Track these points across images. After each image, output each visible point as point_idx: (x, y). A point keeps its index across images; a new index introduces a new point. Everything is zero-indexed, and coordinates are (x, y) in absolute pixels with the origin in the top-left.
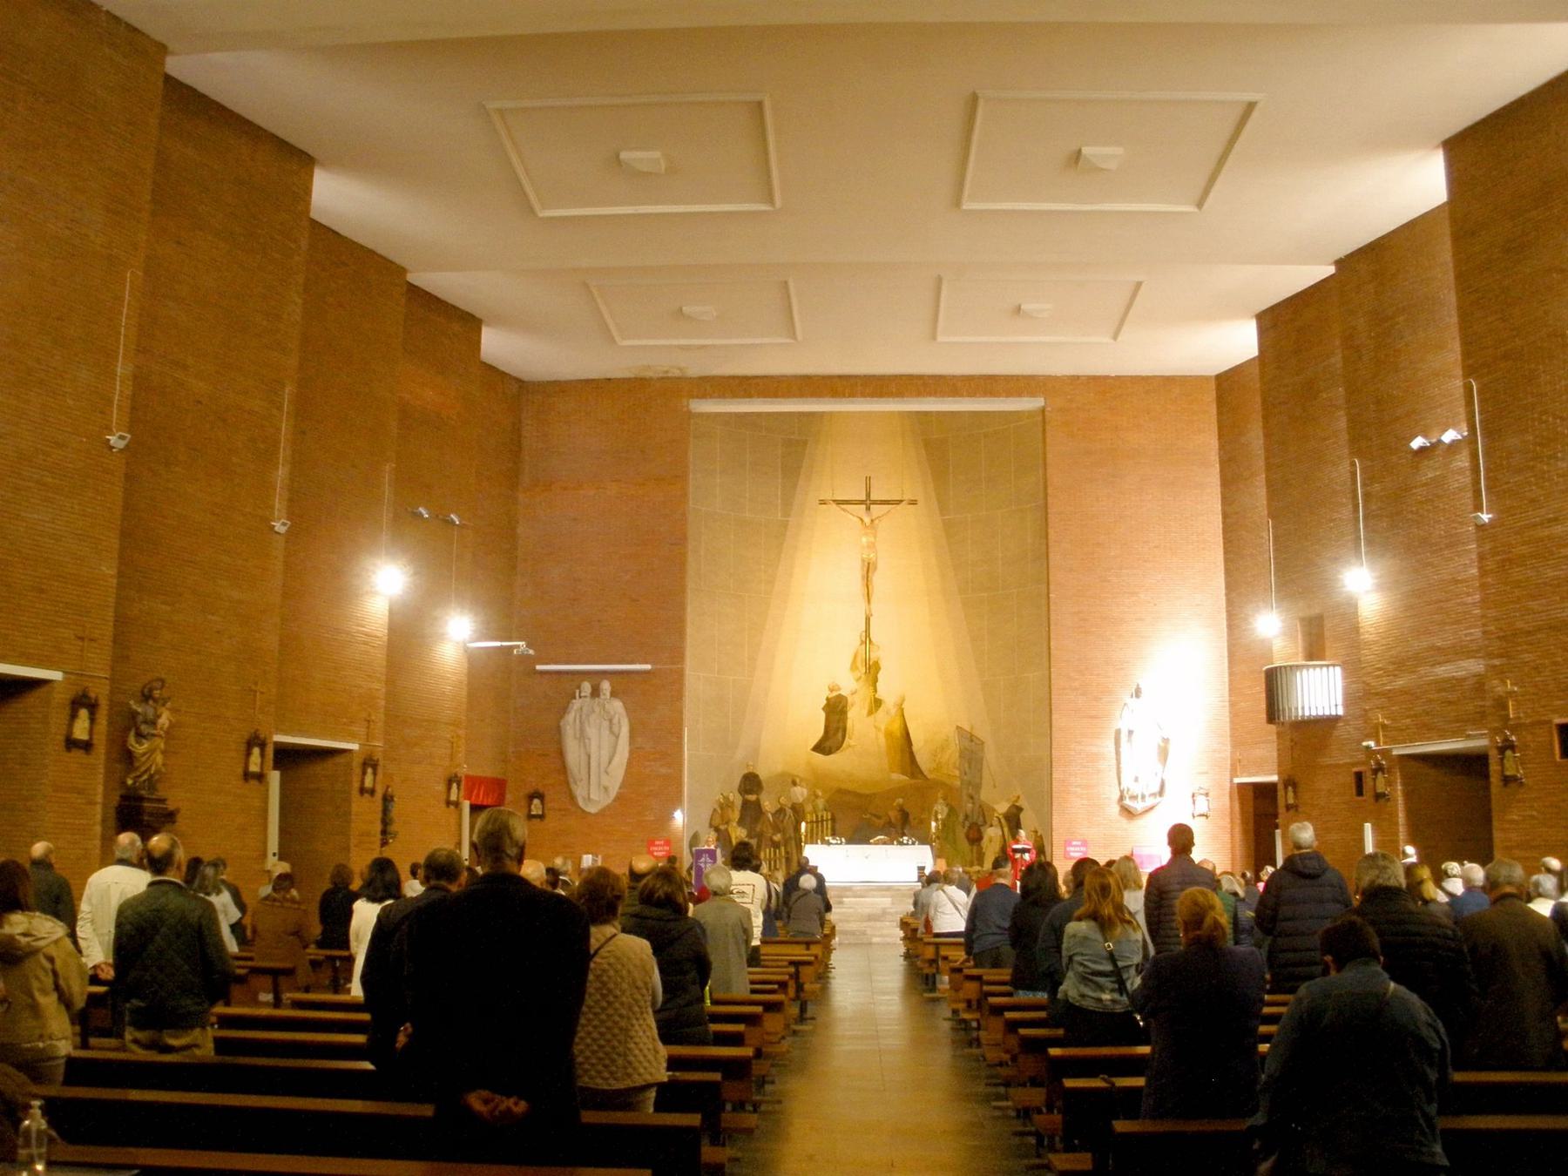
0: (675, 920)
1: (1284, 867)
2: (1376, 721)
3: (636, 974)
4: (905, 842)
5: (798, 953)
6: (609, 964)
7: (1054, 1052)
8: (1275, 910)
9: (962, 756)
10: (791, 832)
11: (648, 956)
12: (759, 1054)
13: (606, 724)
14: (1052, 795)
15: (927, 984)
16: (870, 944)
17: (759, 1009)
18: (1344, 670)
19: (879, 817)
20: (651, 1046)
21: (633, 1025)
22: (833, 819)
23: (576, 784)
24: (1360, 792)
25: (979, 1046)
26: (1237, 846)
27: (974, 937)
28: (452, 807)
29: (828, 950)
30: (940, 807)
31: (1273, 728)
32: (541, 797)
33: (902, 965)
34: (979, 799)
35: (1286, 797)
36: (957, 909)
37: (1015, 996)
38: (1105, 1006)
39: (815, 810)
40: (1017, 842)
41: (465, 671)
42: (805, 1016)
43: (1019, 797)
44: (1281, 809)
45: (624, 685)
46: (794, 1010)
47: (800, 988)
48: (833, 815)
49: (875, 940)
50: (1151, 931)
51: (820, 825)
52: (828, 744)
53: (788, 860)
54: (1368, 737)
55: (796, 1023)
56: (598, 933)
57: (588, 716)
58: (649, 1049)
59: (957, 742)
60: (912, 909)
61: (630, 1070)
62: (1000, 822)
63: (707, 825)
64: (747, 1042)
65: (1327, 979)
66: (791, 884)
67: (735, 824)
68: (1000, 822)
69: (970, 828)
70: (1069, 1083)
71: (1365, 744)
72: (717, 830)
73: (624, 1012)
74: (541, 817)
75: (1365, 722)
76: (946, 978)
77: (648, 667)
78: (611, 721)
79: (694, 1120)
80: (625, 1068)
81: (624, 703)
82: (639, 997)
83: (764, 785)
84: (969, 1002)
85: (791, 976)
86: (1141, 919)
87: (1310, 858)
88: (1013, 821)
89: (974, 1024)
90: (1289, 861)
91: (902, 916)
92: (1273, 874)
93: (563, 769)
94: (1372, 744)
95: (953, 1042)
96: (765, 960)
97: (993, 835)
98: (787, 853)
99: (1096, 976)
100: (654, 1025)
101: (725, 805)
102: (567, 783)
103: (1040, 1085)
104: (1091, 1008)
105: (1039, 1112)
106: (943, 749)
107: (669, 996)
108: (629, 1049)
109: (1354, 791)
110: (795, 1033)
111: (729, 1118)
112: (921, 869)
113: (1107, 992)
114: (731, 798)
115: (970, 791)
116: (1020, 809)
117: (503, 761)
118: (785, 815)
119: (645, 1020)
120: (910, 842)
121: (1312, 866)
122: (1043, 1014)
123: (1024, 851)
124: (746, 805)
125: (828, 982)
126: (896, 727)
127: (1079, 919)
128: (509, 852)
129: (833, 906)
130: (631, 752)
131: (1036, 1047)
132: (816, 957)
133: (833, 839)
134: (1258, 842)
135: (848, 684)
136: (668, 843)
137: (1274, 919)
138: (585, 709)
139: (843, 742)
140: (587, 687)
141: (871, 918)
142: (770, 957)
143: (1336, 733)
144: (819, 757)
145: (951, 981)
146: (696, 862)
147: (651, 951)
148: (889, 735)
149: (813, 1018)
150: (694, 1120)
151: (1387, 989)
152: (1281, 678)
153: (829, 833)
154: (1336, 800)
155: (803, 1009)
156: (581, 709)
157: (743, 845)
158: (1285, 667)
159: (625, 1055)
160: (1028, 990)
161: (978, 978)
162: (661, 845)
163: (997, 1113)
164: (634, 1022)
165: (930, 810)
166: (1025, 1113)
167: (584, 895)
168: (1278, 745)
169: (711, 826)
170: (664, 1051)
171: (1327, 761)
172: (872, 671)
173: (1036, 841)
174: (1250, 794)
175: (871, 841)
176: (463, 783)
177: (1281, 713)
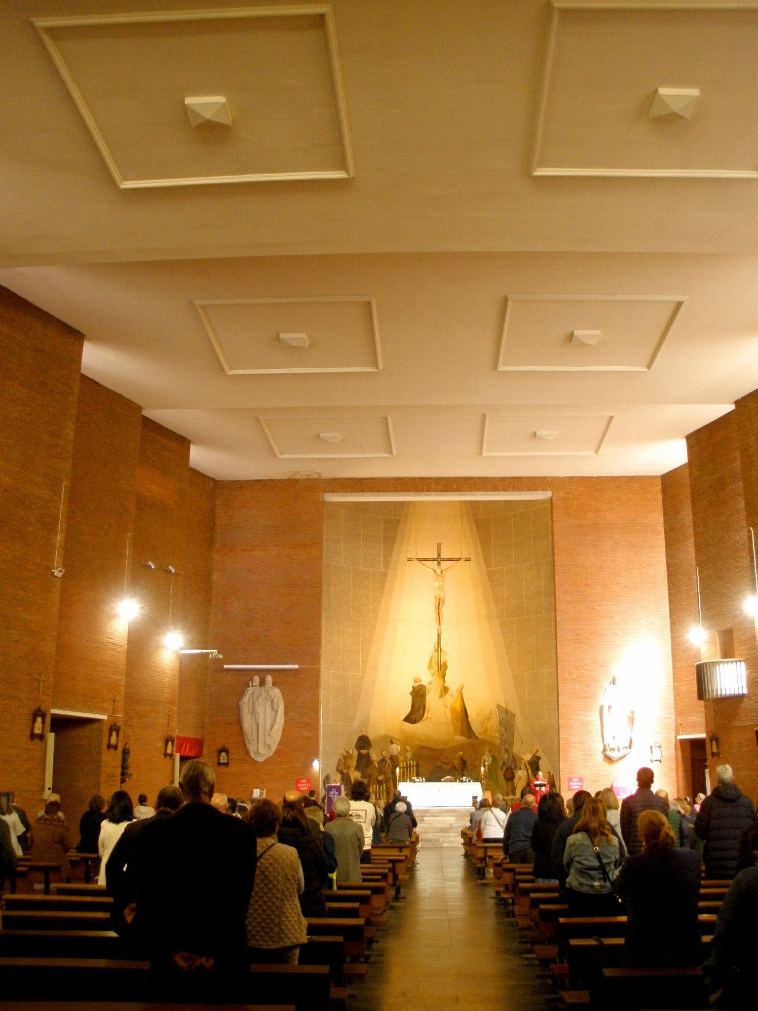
3: (287, 870)
5: (394, 854)
9: (501, 723)
12: (368, 922)
13: (269, 703)
16: (442, 847)
19: (447, 764)
22: (417, 766)
25: (514, 916)
28: (168, 757)
29: (414, 852)
31: (702, 702)
32: (226, 751)
38: (596, 890)
40: (537, 779)
44: (709, 757)
46: (391, 893)
47: (396, 877)
48: (417, 762)
52: (413, 716)
53: (388, 793)
56: (262, 843)
57: (258, 698)
58: (295, 921)
61: (283, 935)
62: (526, 767)
66: (390, 809)
67: (353, 769)
68: (526, 767)
72: (342, 773)
73: (279, 895)
74: (227, 764)
76: (492, 870)
78: (272, 702)
79: (325, 969)
81: (281, 690)
84: (507, 886)
85: (390, 870)
86: (618, 830)
88: (534, 764)
89: (510, 901)
90: (716, 791)
97: (521, 775)
98: (387, 788)
101: (347, 757)
102: (244, 741)
105: (555, 962)
108: (283, 921)
110: (392, 908)
112: (475, 798)
113: (597, 880)
114: (351, 752)
116: (539, 758)
117: (202, 727)
118: (386, 763)
119: (293, 901)
120: (467, 781)
123: (541, 785)
124: (360, 756)
125: (415, 874)
126: (458, 706)
127: (577, 831)
130: (285, 722)
131: (549, 917)
132: (406, 857)
134: (695, 783)
135: (427, 678)
136: (309, 781)
140: (257, 679)
141: (443, 830)
143: (743, 705)
144: (407, 725)
148: (453, 710)
149: (404, 898)
150: (325, 969)
154: (745, 749)
156: (253, 693)
157: (359, 784)
158: (709, 663)
159: (279, 924)
161: (512, 870)
162: (305, 783)
163: (526, 962)
166: (545, 962)
169: (338, 770)
170: (305, 922)
171: (737, 724)
172: (442, 669)
175: (442, 780)
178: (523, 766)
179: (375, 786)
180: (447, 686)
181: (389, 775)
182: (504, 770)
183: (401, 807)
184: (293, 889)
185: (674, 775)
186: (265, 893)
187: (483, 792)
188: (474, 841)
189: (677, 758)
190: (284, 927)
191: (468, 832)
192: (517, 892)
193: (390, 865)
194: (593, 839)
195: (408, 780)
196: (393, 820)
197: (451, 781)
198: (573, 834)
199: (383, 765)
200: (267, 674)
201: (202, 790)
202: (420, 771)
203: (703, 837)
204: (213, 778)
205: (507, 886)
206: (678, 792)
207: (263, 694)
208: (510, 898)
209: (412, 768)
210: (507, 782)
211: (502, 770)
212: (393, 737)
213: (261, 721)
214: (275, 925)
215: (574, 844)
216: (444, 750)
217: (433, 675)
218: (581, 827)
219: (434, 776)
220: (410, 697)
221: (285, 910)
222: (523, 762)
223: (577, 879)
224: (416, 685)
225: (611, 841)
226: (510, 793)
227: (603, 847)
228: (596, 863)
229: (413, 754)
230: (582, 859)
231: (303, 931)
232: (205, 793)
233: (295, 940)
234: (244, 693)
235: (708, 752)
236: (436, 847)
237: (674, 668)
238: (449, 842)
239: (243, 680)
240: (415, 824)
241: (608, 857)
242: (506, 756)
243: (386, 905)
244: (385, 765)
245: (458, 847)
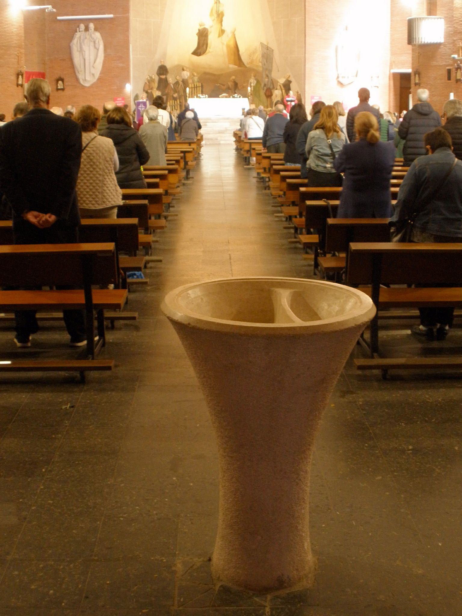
0: (126, 130)
1: (413, 109)
2: (458, 45)
3: (106, 155)
4: (236, 96)
5: (185, 147)
6: (94, 151)
7: (302, 189)
8: (408, 129)
9: (263, 56)
10: (182, 93)
11: (111, 146)
12: (166, 193)
13: (92, 44)
14: (305, 75)
15: (246, 162)
16: (220, 144)
17: (166, 172)
18: (445, 20)
19: (224, 85)
20: (114, 188)
21: (105, 179)
22: (202, 86)
23: (79, 73)
24: (449, 79)
25: (269, 189)
26: (392, 101)
27: (267, 138)
28: (20, 87)
29: (200, 146)
30: (252, 80)
31: (410, 46)
32: (62, 80)
33: (234, 154)
34: (271, 77)
35: (415, 80)
36: (259, 126)
37: (285, 165)
38: (327, 169)
39: (193, 82)
40: (289, 97)
41: (22, 21)
42: (189, 177)
43: (289, 76)
44: (413, 85)
45: (100, 25)
46: (184, 174)
47: (186, 163)
48: (202, 84)
49: (222, 142)
50: (349, 136)
51: (196, 89)
52: (199, 51)
53: (181, 106)
54: (454, 53)
55: (185, 180)
56: (86, 137)
57: (84, 40)
58: (113, 190)
59: (261, 50)
60: (240, 128)
61: (105, 200)
62: (281, 87)
63: (142, 91)
64: (160, 187)
65: (427, 156)
66: (181, 117)
67: (155, 89)
68: (281, 87)
69: (267, 90)
70: (309, 203)
71: (453, 56)
72: (147, 92)
73: (101, 173)
74: (63, 90)
75: (454, 46)
76: (254, 159)
77: (111, 16)
78: (94, 42)
79: (134, 221)
80: (102, 198)
81: (101, 34)
82: (108, 165)
83: (169, 70)
84: (265, 169)
85: (181, 158)
86: (345, 130)
87: (425, 106)
88: (287, 87)
89: (267, 180)
90: (415, 107)
91: (234, 131)
92: (407, 114)
93: (73, 66)
94: (456, 56)
95: (258, 187)
96: (169, 151)
97: (277, 94)
98: (180, 102)
99: (323, 156)
100: (115, 178)
101: (150, 81)
102: (75, 72)
103: (296, 205)
104: (321, 171)
105: (296, 217)
106: (254, 53)
107: (122, 167)
108: (104, 190)
109: (446, 78)
110: (184, 184)
111: (153, 222)
112: (244, 109)
113: (329, 163)
114: (153, 77)
115: (267, 73)
116: (290, 82)
117: (43, 64)
118: (179, 85)
119: (111, 176)
120: (238, 97)
121: (425, 110)
122: (299, 173)
123: (291, 101)
124: (160, 80)
125: (200, 162)
126: (232, 43)
127: (317, 128)
128: (42, 99)
129: (202, 126)
130: (105, 57)
131: (294, 187)
132: (194, 149)
133: (202, 95)
134: (402, 103)
135: (209, 23)
136: (123, 99)
137: (407, 133)
138: (82, 37)
139: (206, 50)
140: (82, 26)
141: (220, 132)
142: (173, 150)
143: (440, 50)
144: (195, 57)
145: (257, 160)
146: (137, 108)
147: (113, 144)
148: (228, 46)
149: (193, 178)
150: (134, 221)
151: (454, 161)
152: (415, 24)
153: (200, 93)
154: (438, 82)
155: (188, 172)
156: (80, 37)
157: (159, 98)
158: (418, 18)
159: (102, 193)
160: (292, 163)
161: (269, 158)
162: (120, 100)
163: (277, 219)
164: (106, 177)
165: (248, 81)
166: (290, 218)
167: (81, 118)
168: (413, 55)
169: (144, 91)
170: (120, 191)
171: (434, 63)
172: (220, 16)
173: (298, 96)
174: (398, 78)
175: (220, 96)
176: (24, 75)
177: (414, 39)
178: (278, 87)
179: (171, 101)
180: (224, 29)
181: (182, 93)
182: (265, 90)
183: (189, 115)
184: (111, 168)
185: (387, 97)
186: (91, 171)
187: (250, 105)
188: (242, 139)
189: (389, 86)
190: (106, 194)
191: (238, 133)
192: (272, 172)
193: (182, 155)
194: (328, 134)
195: (195, 97)
196: (184, 123)
197: (226, 97)
198: (313, 130)
199: (177, 86)
200: (90, 22)
201: (40, 99)
202: (204, 90)
203: (404, 138)
204: (49, 90)
205: (265, 169)
206: (389, 107)
207: (88, 37)
208: (267, 178)
209: (198, 88)
210: (267, 98)
211: (264, 90)
212: (184, 66)
213: (87, 57)
214: (99, 192)
215: (314, 137)
216: (222, 74)
217: (213, 20)
218: (320, 126)
219: (214, 94)
220: (196, 38)
221: (105, 182)
222: (279, 84)
223: (315, 162)
224: (201, 28)
225: (340, 136)
226: (269, 106)
227: (334, 140)
228: (329, 151)
229: (199, 78)
230: (319, 148)
231: (119, 196)
232: (43, 102)
233: (113, 203)
234: (73, 37)
235: (413, 82)
236: (216, 144)
237: (391, 21)
238: (224, 140)
239: (73, 26)
240: (200, 127)
241: (337, 147)
242: (267, 80)
243: (179, 183)
244: (179, 86)
245: (231, 144)
